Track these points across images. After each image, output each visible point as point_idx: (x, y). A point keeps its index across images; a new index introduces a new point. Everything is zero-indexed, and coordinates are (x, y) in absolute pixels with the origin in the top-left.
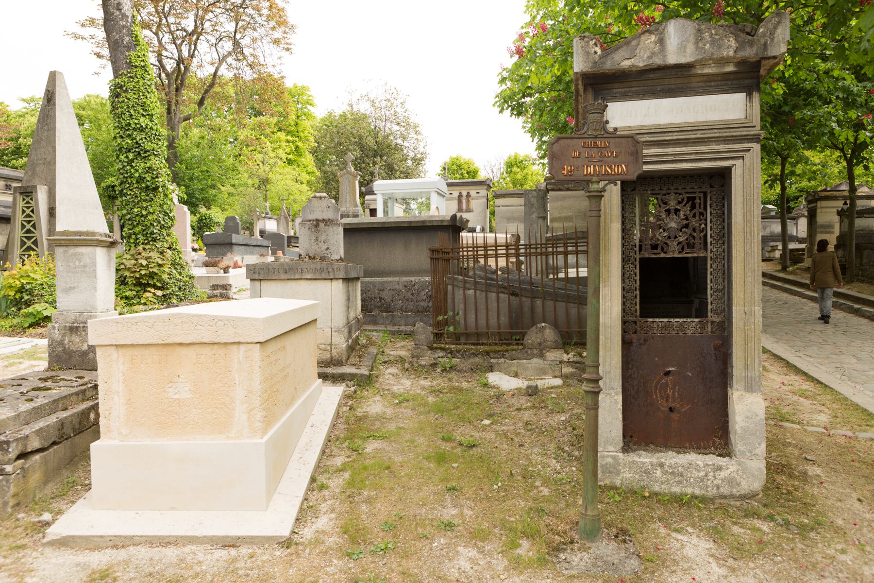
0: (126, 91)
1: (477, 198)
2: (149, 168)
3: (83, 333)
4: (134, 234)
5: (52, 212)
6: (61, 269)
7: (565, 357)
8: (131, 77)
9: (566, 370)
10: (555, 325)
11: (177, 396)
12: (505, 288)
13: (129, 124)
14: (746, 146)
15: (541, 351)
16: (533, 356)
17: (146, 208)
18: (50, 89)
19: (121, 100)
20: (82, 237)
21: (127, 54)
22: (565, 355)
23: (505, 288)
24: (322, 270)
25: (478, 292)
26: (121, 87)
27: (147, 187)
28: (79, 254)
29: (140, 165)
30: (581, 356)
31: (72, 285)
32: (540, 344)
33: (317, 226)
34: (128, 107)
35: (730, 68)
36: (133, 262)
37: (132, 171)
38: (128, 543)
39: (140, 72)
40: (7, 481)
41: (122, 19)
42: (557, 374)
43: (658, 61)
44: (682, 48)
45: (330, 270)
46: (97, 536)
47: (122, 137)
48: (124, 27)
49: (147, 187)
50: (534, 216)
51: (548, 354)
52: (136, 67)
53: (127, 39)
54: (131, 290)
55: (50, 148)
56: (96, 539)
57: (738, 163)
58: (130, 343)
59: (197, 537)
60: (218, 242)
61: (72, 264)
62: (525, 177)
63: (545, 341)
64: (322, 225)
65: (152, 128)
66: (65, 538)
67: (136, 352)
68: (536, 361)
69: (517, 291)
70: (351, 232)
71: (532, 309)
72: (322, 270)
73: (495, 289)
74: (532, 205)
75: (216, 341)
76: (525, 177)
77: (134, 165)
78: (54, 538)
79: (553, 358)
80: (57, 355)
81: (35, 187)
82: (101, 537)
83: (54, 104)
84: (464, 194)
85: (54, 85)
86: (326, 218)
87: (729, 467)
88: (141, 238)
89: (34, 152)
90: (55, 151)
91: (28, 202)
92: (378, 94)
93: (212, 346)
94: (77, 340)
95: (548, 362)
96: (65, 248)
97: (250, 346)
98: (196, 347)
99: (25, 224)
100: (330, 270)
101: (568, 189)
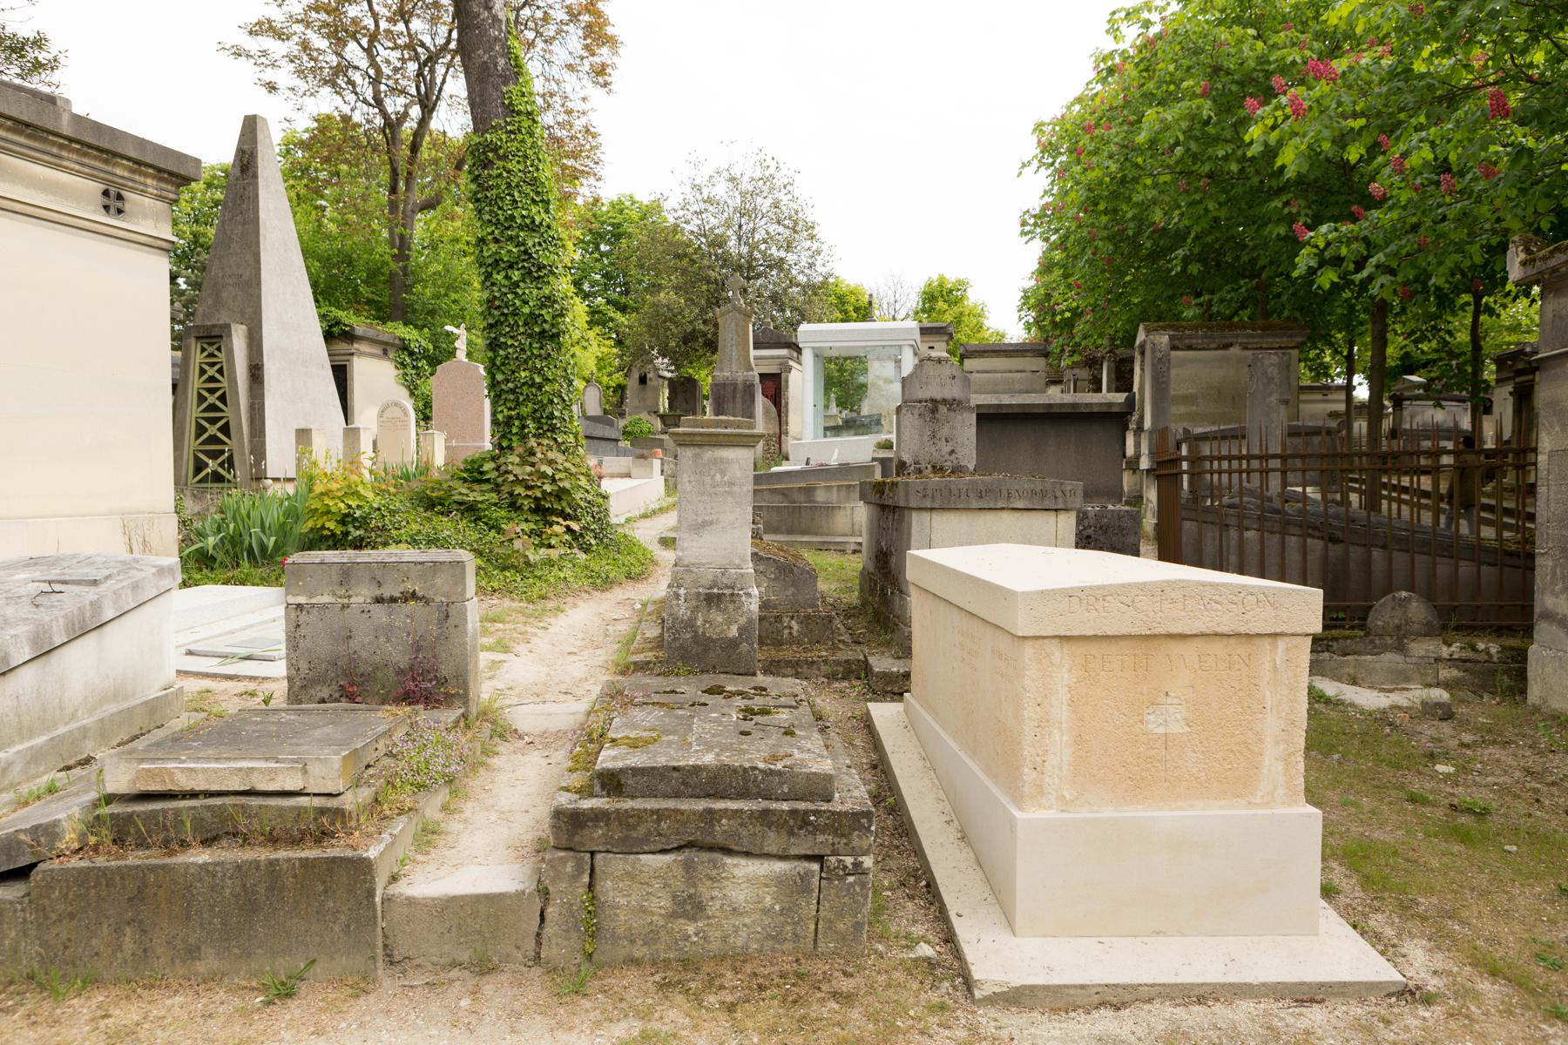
0: (504, 158)
2: (548, 298)
3: (731, 607)
4: (519, 417)
5: (256, 373)
6: (689, 488)
7: (1445, 651)
8: (511, 132)
9: (1446, 673)
10: (1429, 596)
11: (1161, 730)
12: (1316, 528)
13: (512, 218)
15: (1399, 640)
16: (1385, 648)
17: (540, 371)
18: (246, 147)
19: (495, 172)
20: (729, 431)
21: (505, 89)
22: (1445, 648)
23: (1316, 528)
24: (1044, 494)
26: (495, 150)
27: (543, 332)
29: (531, 291)
30: (1474, 649)
32: (1399, 628)
33: (934, 411)
34: (509, 185)
36: (529, 469)
37: (518, 303)
38: (1127, 998)
39: (526, 124)
40: (863, 886)
41: (492, 26)
42: (1429, 680)
45: (1059, 493)
46: (1075, 986)
47: (496, 241)
48: (496, 39)
49: (543, 332)
50: (1274, 398)
51: (1413, 645)
52: (519, 113)
53: (501, 62)
54: (526, 520)
55: (248, 257)
56: (1072, 991)
58: (1091, 633)
59: (1250, 986)
61: (708, 480)
62: (958, 320)
63: (1408, 622)
64: (943, 409)
65: (549, 227)
66: (1017, 989)
67: (1093, 649)
68: (1389, 657)
69: (1339, 534)
70: (990, 419)
71: (1368, 563)
72: (1044, 494)
73: (1297, 530)
74: (1270, 380)
75: (1243, 630)
76: (958, 320)
77: (520, 291)
78: (997, 990)
79: (1422, 653)
80: (682, 646)
81: (227, 327)
82: (1082, 987)
83: (255, 176)
85: (254, 141)
86: (948, 396)
88: (531, 424)
89: (217, 263)
90: (258, 262)
91: (211, 355)
92: (747, 170)
93: (1225, 640)
94: (720, 619)
95: (1414, 660)
96: (697, 450)
97: (1296, 640)
98: (1198, 643)
99: (206, 394)
100: (1059, 493)
101: (1190, 348)
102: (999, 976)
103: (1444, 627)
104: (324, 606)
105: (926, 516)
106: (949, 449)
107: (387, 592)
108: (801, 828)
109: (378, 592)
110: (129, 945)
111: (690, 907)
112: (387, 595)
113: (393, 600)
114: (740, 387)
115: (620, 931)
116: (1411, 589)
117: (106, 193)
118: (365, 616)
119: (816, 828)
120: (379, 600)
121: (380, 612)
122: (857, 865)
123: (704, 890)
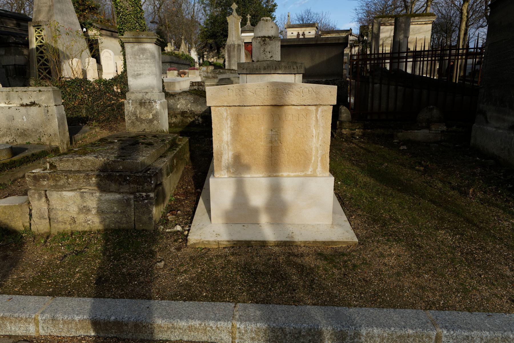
3: (149, 107)
16: (423, 128)
25: (383, 85)
31: (139, 73)
84: (301, 33)
86: (270, 35)
105: (245, 76)
106: (270, 56)
108: (124, 182)
109: (21, 102)
112: (25, 104)
113: (27, 105)
114: (236, 45)
118: (18, 111)
119: (130, 182)
120: (22, 105)
121: (23, 110)
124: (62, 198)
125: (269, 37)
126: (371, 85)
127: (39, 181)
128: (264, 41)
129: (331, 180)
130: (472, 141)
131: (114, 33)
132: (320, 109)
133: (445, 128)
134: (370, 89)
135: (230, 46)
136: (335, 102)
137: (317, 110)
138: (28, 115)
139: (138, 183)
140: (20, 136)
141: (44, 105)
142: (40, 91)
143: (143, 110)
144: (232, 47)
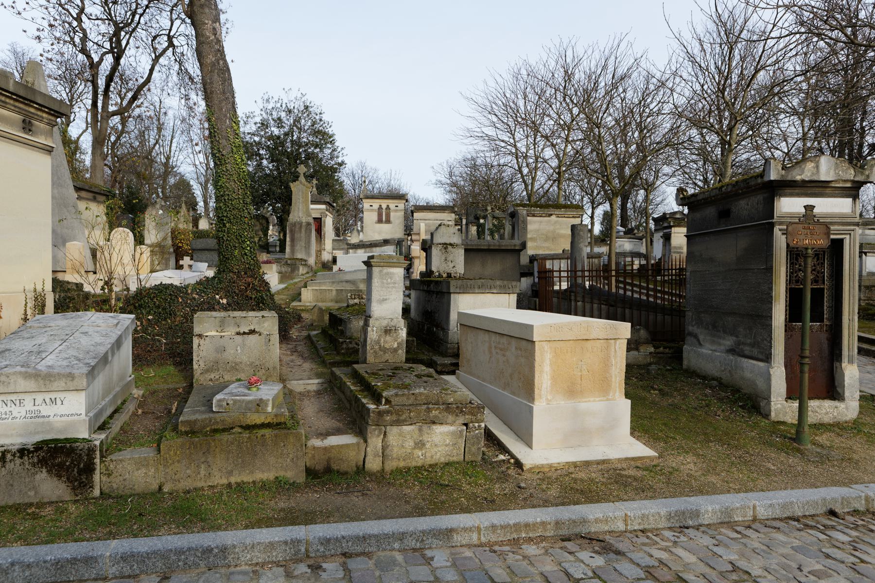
1: (396, 211)
14: (852, 228)
28: (391, 273)
35: (849, 185)
43: (815, 178)
44: (828, 173)
57: (848, 237)
60: (208, 247)
84: (384, 206)
87: (841, 406)
102: (532, 462)
103: (653, 340)
104: (213, 337)
105: (456, 295)
107: (243, 329)
109: (238, 330)
110: (203, 472)
111: (420, 445)
112: (242, 331)
113: (244, 333)
115: (394, 456)
116: (640, 325)
117: (24, 121)
120: (238, 334)
122: (479, 426)
123: (425, 438)
124: (400, 434)
125: (451, 244)
126: (573, 303)
127: (382, 416)
128: (445, 248)
129: (626, 405)
130: (685, 363)
131: (97, 196)
132: (618, 342)
133: (652, 350)
134: (573, 307)
135: (294, 225)
136: (629, 336)
137: (615, 343)
138: (244, 345)
139: (472, 414)
140: (229, 371)
141: (265, 333)
142: (263, 317)
143: (388, 338)
144: (298, 226)
